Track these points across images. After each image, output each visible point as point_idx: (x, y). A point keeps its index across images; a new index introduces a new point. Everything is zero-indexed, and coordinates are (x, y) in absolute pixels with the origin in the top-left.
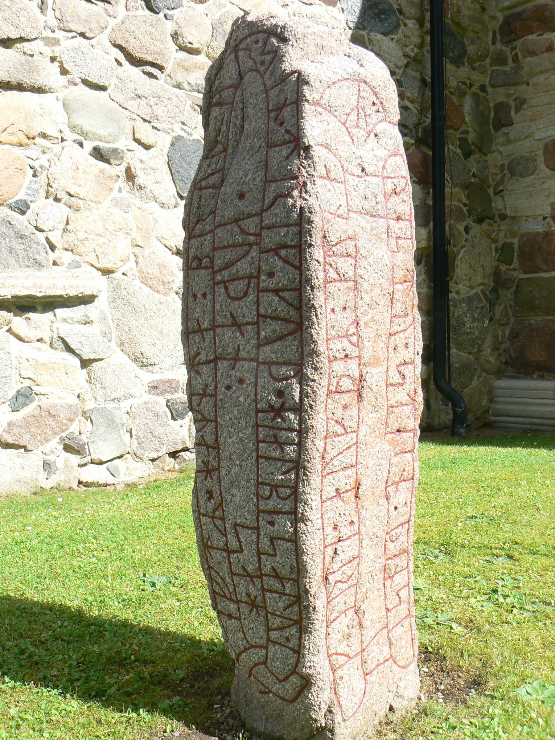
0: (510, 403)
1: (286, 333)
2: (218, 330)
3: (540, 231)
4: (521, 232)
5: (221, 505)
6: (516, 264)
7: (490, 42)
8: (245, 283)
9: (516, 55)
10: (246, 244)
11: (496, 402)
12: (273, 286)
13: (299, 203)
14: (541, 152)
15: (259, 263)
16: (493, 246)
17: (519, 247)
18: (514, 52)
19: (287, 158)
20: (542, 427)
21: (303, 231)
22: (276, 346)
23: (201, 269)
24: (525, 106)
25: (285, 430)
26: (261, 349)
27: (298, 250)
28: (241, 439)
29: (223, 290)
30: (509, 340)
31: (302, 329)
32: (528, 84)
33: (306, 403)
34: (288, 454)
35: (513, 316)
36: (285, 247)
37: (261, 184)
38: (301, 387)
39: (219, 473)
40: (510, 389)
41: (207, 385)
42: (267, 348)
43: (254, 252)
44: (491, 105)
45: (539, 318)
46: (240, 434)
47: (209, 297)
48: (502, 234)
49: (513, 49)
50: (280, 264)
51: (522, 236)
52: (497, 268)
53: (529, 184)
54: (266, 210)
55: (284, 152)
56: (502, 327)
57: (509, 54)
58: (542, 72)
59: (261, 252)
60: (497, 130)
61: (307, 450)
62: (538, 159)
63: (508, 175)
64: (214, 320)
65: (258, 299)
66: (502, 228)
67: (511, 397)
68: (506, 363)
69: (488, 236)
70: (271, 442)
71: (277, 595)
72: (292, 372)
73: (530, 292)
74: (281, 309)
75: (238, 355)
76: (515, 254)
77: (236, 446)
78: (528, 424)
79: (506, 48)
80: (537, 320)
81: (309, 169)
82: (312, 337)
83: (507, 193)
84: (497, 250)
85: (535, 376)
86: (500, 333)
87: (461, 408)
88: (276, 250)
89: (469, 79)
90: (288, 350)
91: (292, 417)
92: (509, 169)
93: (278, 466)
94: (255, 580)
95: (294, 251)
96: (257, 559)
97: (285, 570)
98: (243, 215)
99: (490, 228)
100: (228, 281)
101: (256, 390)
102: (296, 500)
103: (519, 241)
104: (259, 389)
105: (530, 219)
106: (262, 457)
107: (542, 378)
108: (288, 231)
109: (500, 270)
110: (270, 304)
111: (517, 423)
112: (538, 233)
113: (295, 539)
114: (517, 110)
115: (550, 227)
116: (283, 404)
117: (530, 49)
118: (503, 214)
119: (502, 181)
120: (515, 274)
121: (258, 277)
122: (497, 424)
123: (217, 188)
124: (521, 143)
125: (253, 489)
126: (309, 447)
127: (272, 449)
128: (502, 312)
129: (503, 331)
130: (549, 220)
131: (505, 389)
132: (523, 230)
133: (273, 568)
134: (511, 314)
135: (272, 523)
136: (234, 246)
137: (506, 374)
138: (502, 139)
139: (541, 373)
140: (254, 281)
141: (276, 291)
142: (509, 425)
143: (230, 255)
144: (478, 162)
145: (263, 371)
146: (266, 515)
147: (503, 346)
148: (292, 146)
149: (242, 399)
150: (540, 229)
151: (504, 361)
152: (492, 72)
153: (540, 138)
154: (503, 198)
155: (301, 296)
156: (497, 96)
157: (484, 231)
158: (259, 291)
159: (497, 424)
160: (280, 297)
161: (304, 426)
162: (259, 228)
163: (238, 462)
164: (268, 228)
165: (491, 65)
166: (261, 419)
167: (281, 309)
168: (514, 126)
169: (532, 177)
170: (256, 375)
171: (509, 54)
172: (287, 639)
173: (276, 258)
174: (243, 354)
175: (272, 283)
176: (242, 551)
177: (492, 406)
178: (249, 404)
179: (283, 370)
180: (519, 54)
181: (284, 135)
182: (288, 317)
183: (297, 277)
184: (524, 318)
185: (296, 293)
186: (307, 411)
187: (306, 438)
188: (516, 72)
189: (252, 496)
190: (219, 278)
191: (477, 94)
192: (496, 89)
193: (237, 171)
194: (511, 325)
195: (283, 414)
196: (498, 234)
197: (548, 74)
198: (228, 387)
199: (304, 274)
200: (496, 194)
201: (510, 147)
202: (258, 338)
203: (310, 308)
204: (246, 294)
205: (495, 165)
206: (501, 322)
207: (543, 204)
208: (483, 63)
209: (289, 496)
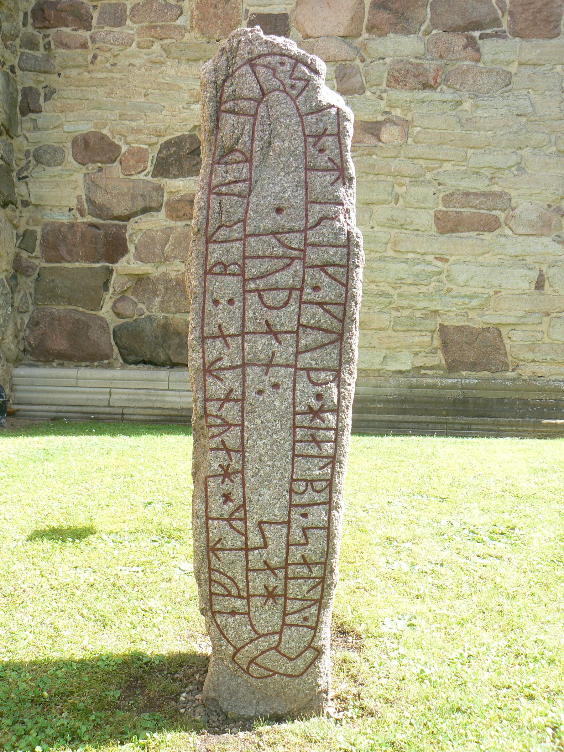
0: (36, 391)
1: (326, 342)
2: (247, 337)
3: (66, 222)
4: (44, 220)
5: (243, 506)
6: (38, 251)
7: (21, 23)
8: (286, 294)
9: (49, 43)
10: (287, 258)
11: (16, 391)
12: (319, 299)
13: (346, 228)
14: (69, 145)
15: (304, 277)
16: (15, 232)
17: (43, 236)
18: (47, 40)
19: (332, 184)
20: (69, 415)
21: (352, 253)
22: (317, 353)
23: (226, 274)
24: (55, 96)
25: (323, 429)
26: (299, 356)
27: (346, 269)
28: (275, 441)
29: (257, 298)
30: (29, 328)
31: (342, 339)
32: (59, 75)
33: (344, 404)
34: (326, 450)
35: (32, 304)
36: (333, 265)
37: (302, 203)
38: (339, 391)
39: (243, 475)
40: (29, 377)
41: (231, 391)
42: (307, 355)
43: (297, 266)
44: (20, 88)
45: (61, 308)
46: (274, 436)
47: (238, 304)
48: (23, 221)
49: (46, 36)
50: (327, 280)
51: (46, 225)
52: (17, 255)
53: (56, 174)
54: (311, 228)
55: (328, 178)
56: (21, 315)
57: (41, 41)
58: (75, 67)
59: (304, 267)
60: (23, 114)
61: (343, 445)
62: (66, 151)
63: (33, 162)
64: (243, 326)
65: (300, 310)
66: (23, 215)
67: (32, 385)
68: (24, 351)
69: (11, 221)
70: (308, 441)
71: (302, 581)
72: (331, 377)
73: (53, 281)
74: (325, 321)
75: (271, 361)
76: (38, 242)
77: (269, 447)
78: (54, 412)
79: (38, 34)
80: (59, 308)
81: (351, 198)
82: (351, 347)
83: (32, 180)
84: (18, 236)
85: (55, 364)
86: (19, 321)
87: (3, 398)
88: (323, 267)
89: (3, 57)
90: (328, 357)
91: (331, 417)
92: (34, 156)
93: (316, 462)
94: (276, 571)
95: (342, 270)
96: (284, 551)
97: (315, 555)
98: (283, 229)
99: (13, 213)
100: (264, 290)
101: (294, 394)
102: (331, 491)
103: (43, 230)
104: (298, 393)
105: (54, 209)
106: (298, 456)
107: (62, 365)
108: (337, 252)
109: (21, 257)
110: (314, 316)
111: (42, 411)
112: (63, 223)
113: (328, 528)
114: (46, 99)
115: (76, 219)
116: (322, 406)
117: (64, 42)
118: (27, 201)
119: (27, 167)
120: (37, 262)
121: (301, 290)
122: (20, 413)
123: (244, 197)
124: (49, 132)
125: (287, 486)
126: (344, 443)
127: (309, 447)
128: (21, 299)
129: (21, 319)
130: (74, 212)
131: (25, 377)
132: (47, 219)
133: (303, 556)
134: (30, 301)
135: (305, 515)
136: (271, 257)
137: (23, 362)
138: (29, 125)
139: (61, 362)
140: (295, 294)
141: (321, 304)
142: (33, 413)
143: (267, 265)
144: (5, 145)
145: (302, 377)
146: (300, 508)
147: (22, 334)
148: (337, 174)
149: (277, 403)
150: (65, 220)
151: (22, 349)
152: (22, 54)
153: (69, 130)
154: (27, 183)
155: (345, 310)
156: (26, 80)
157: (7, 216)
158: (301, 302)
159: (20, 413)
160: (324, 309)
161: (340, 425)
162: (303, 244)
163: (269, 463)
164: (314, 245)
165: (21, 47)
166: (301, 420)
167: (325, 321)
168: (42, 113)
169: (60, 167)
170: (295, 379)
171: (41, 41)
172: (306, 619)
173: (323, 274)
174: (279, 360)
175: (319, 296)
176: (266, 546)
177: (13, 394)
178: (286, 408)
179: (323, 375)
180: (52, 43)
181: (327, 162)
182: (330, 328)
183: (344, 292)
184: (45, 307)
185: (341, 308)
186: (344, 412)
187: (342, 435)
188: (48, 60)
189: (285, 493)
190: (252, 286)
191: (8, 73)
192: (26, 72)
193: (271, 185)
194: (30, 313)
195: (321, 415)
196: (19, 220)
197: (81, 70)
198: (260, 392)
199: (350, 292)
200: (19, 179)
201: (37, 134)
202: (297, 346)
203: (353, 321)
204: (286, 304)
205: (20, 150)
206: (21, 310)
207: (69, 196)
208: (14, 43)
209: (325, 488)
